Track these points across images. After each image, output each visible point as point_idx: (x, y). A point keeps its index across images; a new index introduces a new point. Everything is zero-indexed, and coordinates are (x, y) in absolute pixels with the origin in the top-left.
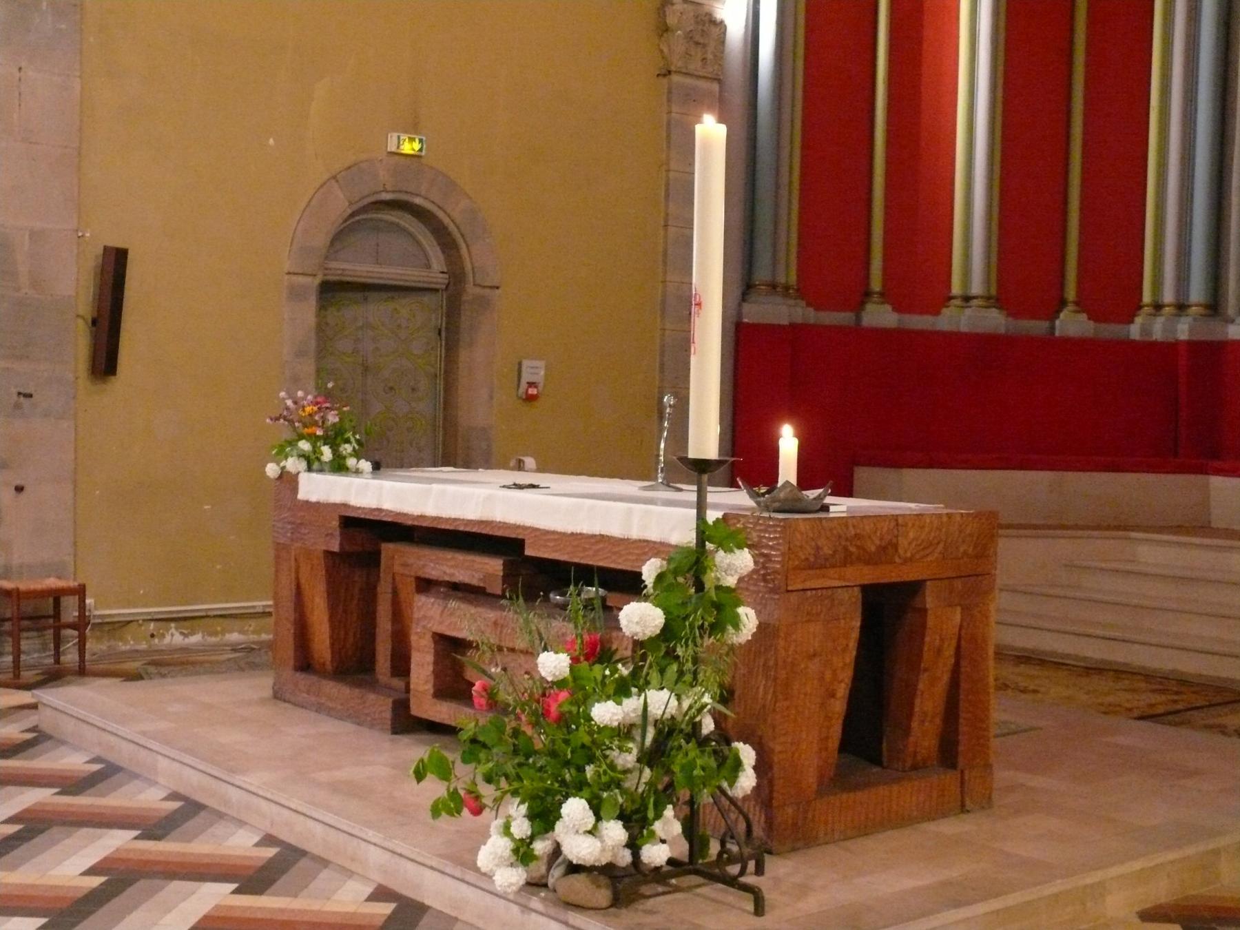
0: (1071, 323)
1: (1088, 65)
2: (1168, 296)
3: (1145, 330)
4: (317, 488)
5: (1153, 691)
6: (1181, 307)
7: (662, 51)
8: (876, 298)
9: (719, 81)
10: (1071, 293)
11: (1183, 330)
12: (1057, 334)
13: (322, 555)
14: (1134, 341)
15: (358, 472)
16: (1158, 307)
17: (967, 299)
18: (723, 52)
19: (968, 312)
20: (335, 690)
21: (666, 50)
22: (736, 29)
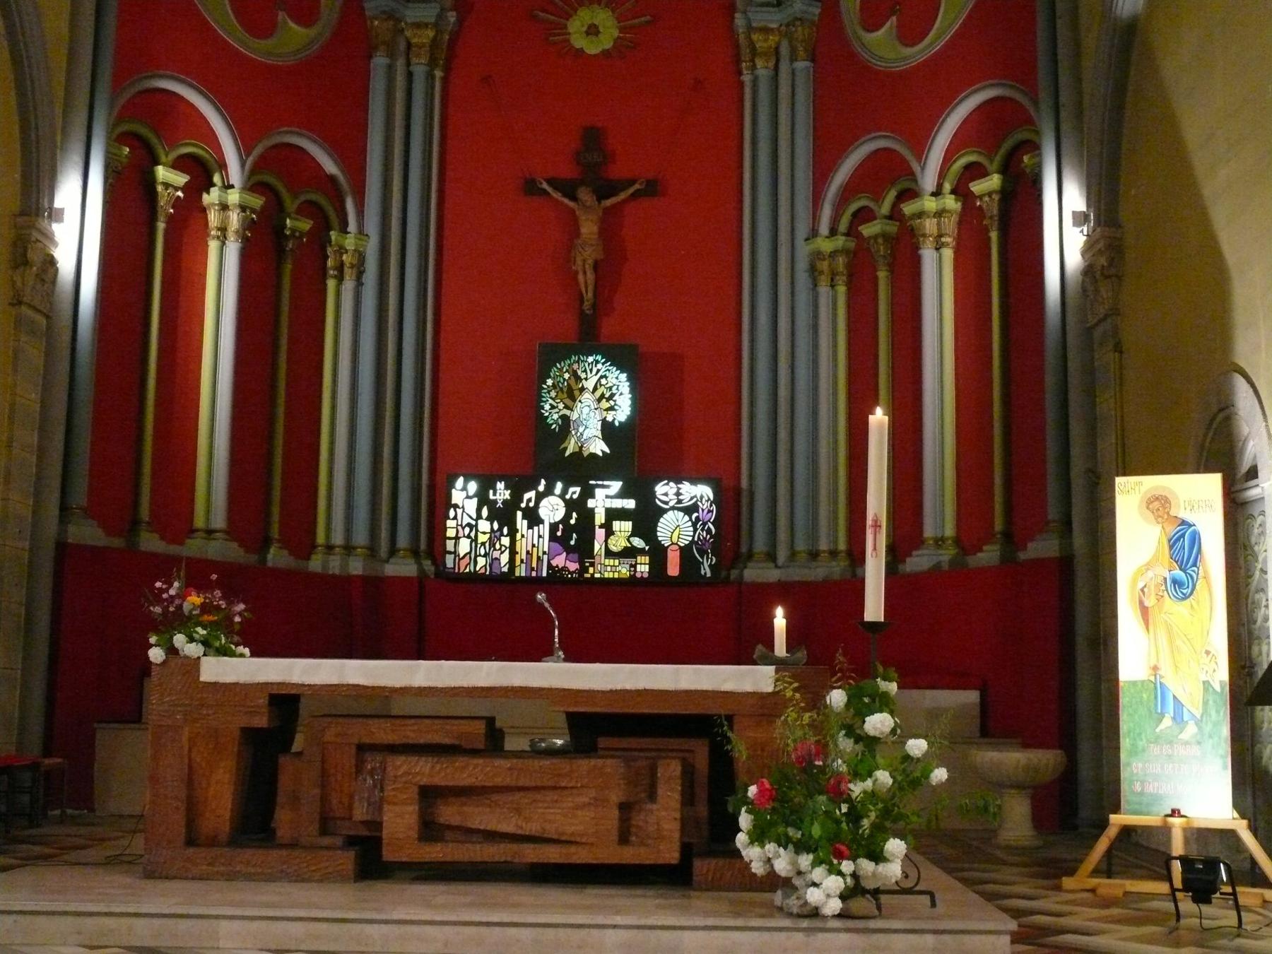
0: (277, 557)
1: (990, 269)
2: (338, 539)
3: (325, 565)
4: (215, 670)
5: (1065, 861)
6: (349, 548)
7: (14, 283)
8: (144, 526)
9: (48, 317)
10: (275, 531)
11: (356, 567)
12: (270, 564)
13: (237, 733)
14: (333, 576)
15: (242, 655)
16: (330, 548)
17: (210, 532)
18: (53, 292)
19: (213, 543)
20: (251, 856)
21: (19, 284)
22: (66, 265)
